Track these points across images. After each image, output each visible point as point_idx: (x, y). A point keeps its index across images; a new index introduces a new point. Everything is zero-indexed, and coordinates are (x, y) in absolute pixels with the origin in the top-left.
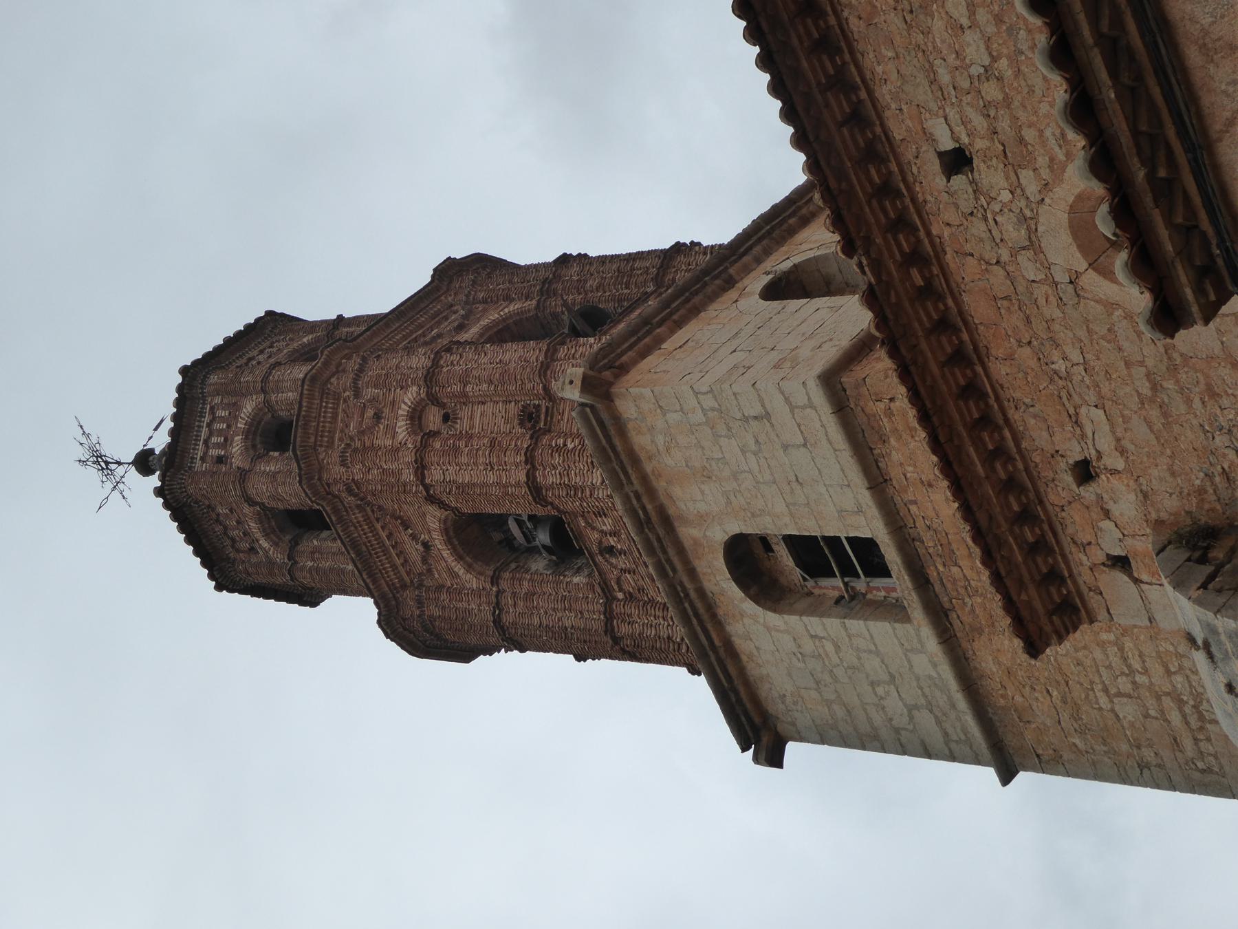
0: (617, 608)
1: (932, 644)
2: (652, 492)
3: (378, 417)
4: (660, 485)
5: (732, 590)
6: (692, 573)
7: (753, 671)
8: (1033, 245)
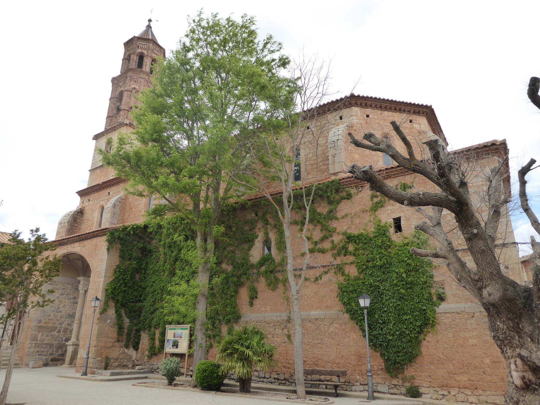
2: (118, 129)
6: (110, 132)
7: (102, 138)
8: (103, 200)
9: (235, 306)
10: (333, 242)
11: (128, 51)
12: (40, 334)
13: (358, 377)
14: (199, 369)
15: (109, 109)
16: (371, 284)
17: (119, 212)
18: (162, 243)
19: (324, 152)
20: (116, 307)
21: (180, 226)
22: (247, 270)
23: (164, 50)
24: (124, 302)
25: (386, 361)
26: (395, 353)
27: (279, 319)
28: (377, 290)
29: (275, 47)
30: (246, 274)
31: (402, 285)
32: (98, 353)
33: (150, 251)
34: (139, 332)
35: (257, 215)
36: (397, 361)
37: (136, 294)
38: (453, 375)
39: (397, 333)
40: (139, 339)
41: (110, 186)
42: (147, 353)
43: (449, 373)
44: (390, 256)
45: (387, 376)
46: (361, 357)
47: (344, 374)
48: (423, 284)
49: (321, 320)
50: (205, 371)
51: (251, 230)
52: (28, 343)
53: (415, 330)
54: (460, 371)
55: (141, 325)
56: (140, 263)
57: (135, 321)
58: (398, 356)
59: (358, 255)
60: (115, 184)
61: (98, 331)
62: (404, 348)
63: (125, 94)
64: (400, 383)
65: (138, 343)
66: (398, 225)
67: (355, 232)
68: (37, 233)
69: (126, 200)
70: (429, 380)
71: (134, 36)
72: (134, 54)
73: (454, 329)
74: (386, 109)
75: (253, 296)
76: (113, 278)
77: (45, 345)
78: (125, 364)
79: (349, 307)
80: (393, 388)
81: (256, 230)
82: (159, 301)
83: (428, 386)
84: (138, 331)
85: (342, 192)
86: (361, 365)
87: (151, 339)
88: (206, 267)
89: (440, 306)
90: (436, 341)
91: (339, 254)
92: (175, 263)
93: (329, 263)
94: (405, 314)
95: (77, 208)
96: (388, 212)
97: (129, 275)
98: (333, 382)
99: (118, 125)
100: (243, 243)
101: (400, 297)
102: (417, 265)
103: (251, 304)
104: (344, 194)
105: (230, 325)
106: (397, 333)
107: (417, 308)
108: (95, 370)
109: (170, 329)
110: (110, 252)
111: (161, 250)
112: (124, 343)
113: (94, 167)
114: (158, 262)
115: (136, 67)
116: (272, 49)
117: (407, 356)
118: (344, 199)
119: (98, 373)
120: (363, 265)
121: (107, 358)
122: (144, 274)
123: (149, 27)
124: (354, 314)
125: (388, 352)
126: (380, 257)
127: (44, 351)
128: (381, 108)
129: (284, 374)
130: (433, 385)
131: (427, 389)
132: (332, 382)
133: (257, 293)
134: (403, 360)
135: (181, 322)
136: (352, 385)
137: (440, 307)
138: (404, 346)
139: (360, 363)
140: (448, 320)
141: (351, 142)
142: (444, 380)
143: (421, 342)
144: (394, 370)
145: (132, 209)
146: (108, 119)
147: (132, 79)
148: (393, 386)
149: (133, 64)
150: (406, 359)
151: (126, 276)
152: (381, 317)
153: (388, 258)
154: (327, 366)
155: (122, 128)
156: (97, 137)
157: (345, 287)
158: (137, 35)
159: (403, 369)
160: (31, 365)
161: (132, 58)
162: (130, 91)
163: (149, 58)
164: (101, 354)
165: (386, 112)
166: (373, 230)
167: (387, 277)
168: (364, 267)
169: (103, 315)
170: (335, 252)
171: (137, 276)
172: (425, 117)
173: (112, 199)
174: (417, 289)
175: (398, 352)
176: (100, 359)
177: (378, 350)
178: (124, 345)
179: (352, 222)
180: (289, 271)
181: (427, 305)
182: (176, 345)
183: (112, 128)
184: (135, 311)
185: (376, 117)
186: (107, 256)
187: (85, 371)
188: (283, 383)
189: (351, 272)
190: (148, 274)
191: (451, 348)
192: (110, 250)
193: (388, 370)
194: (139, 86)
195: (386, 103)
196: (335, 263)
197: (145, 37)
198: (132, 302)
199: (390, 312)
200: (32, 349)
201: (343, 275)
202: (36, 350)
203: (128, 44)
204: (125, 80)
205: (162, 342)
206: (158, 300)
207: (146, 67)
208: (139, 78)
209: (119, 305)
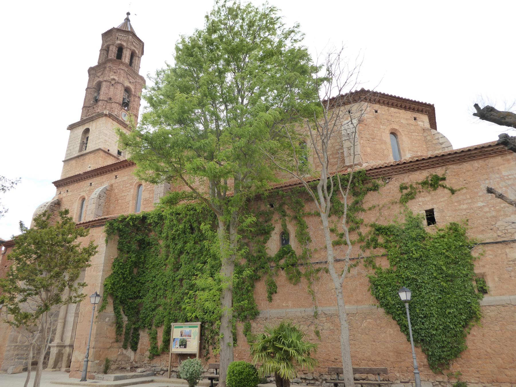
0: (87, 108)
1: (76, 155)
3: (115, 73)
4: (96, 121)
5: (85, 128)
6: (87, 123)
7: (77, 128)
8: (83, 191)
9: (251, 302)
10: (360, 234)
11: (106, 42)
12: (20, 335)
13: (398, 375)
14: (233, 372)
15: (85, 99)
16: (408, 277)
17: (104, 204)
18: (164, 235)
19: (334, 145)
20: (114, 304)
21: (186, 217)
22: (264, 264)
23: (143, 43)
24: (122, 298)
25: (429, 357)
26: (440, 348)
27: (303, 315)
28: (415, 283)
29: (298, 37)
30: (263, 268)
31: (442, 277)
32: (97, 356)
33: (149, 244)
34: (138, 331)
35: (272, 206)
36: (442, 356)
37: (135, 290)
38: (503, 370)
39: (441, 327)
40: (138, 339)
41: (92, 176)
42: (148, 353)
43: (498, 368)
44: (425, 249)
45: (431, 372)
46: (400, 354)
47: (385, 371)
48: (464, 277)
49: (352, 315)
50: (241, 373)
51: (266, 222)
52: (7, 345)
53: (460, 324)
54: (511, 365)
55: (139, 323)
56: (139, 257)
57: (134, 319)
58: (443, 352)
59: (391, 247)
60: (98, 174)
61: (97, 330)
62: (449, 343)
63: (104, 85)
64: (446, 380)
65: (136, 343)
66: (431, 218)
67: (383, 223)
68: (67, 216)
69: (111, 191)
70: (477, 375)
71: (114, 28)
72: (113, 45)
73: (501, 322)
74: (392, 105)
75: (272, 291)
76: (112, 272)
77: (25, 347)
78: (123, 366)
79: (384, 301)
80: (437, 385)
81: (273, 222)
82: (162, 297)
83: (476, 382)
84: (136, 330)
85: (367, 183)
86: (400, 362)
87: (153, 338)
88: (231, 260)
89: (483, 299)
90: (482, 335)
91: (368, 246)
92: (179, 256)
93: (357, 255)
94: (450, 307)
95: (53, 199)
96: (420, 203)
97: (128, 269)
98: (370, 380)
99: (96, 115)
100: (257, 235)
101: (441, 290)
102: (456, 258)
103: (270, 299)
104: (370, 185)
105: (247, 322)
106: (441, 327)
107: (461, 301)
108: (94, 374)
109: (176, 327)
110: (108, 244)
111: (162, 243)
112: (122, 343)
113: (68, 158)
114: (157, 256)
115: (115, 58)
116: (295, 38)
117: (453, 351)
118: (370, 191)
119: (99, 378)
120: (396, 257)
121: (108, 361)
122: (142, 268)
123: (127, 20)
124: (390, 308)
125: (431, 348)
126: (415, 250)
127: (24, 354)
128: (388, 104)
129: (313, 373)
130: (481, 381)
131: (475, 385)
132: (368, 380)
133: (277, 288)
134: (448, 356)
135: (188, 319)
136: (391, 384)
137: (484, 299)
138: (449, 341)
139: (399, 360)
140: (493, 313)
141: (475, 115)
142: (493, 375)
143: (466, 336)
144: (439, 365)
145: (118, 200)
146: (84, 109)
147: (111, 69)
148: (437, 383)
149: (113, 55)
150: (451, 354)
151: (124, 270)
152: (421, 311)
153: (423, 250)
154: (362, 364)
155: (101, 119)
156: (72, 127)
157: (378, 280)
158: (115, 27)
159: (448, 364)
160: (10, 370)
161: (111, 48)
162: (109, 81)
163: (128, 50)
164: (100, 356)
165: (392, 109)
166: (404, 221)
167: (424, 269)
168: (398, 259)
169: (102, 313)
170: (364, 244)
171: (135, 271)
172: (427, 116)
173: (97, 190)
174: (459, 281)
175: (443, 347)
176: (99, 361)
177: (419, 345)
178: (123, 345)
179: (380, 214)
180: (330, 263)
181: (471, 298)
182: (183, 344)
183: (90, 118)
184: (133, 309)
185: (384, 113)
186: (105, 248)
187: (84, 376)
188: (312, 384)
189: (382, 265)
190: (147, 269)
191: (499, 342)
192: (109, 241)
193: (432, 366)
194: (118, 77)
195: (393, 100)
196: (364, 255)
197: (124, 29)
198: (130, 299)
199: (432, 306)
200: (11, 352)
201: (374, 268)
202: (16, 353)
203: (107, 35)
204: (104, 71)
205: (167, 342)
206: (161, 296)
207: (125, 58)
208: (119, 69)
209: (118, 301)
